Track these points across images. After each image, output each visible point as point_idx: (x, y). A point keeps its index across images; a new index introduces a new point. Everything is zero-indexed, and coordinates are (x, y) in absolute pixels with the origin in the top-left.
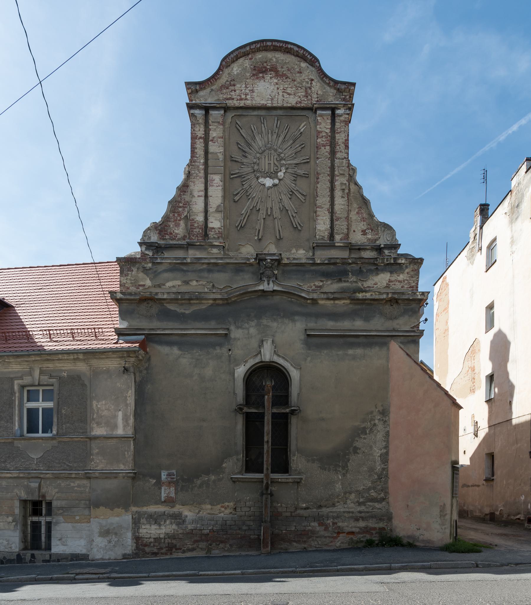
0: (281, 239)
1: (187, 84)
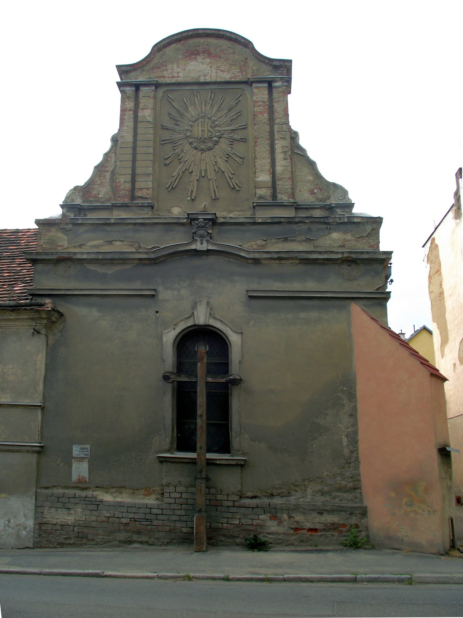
0: (216, 199)
1: (118, 67)
